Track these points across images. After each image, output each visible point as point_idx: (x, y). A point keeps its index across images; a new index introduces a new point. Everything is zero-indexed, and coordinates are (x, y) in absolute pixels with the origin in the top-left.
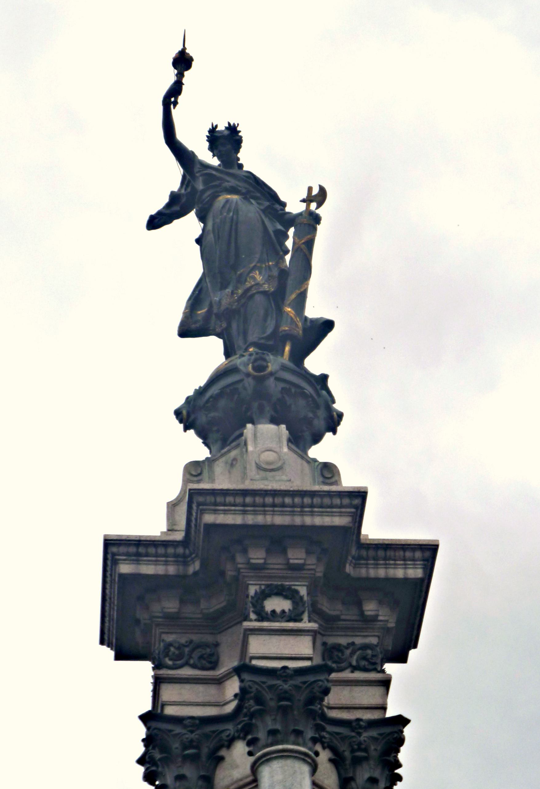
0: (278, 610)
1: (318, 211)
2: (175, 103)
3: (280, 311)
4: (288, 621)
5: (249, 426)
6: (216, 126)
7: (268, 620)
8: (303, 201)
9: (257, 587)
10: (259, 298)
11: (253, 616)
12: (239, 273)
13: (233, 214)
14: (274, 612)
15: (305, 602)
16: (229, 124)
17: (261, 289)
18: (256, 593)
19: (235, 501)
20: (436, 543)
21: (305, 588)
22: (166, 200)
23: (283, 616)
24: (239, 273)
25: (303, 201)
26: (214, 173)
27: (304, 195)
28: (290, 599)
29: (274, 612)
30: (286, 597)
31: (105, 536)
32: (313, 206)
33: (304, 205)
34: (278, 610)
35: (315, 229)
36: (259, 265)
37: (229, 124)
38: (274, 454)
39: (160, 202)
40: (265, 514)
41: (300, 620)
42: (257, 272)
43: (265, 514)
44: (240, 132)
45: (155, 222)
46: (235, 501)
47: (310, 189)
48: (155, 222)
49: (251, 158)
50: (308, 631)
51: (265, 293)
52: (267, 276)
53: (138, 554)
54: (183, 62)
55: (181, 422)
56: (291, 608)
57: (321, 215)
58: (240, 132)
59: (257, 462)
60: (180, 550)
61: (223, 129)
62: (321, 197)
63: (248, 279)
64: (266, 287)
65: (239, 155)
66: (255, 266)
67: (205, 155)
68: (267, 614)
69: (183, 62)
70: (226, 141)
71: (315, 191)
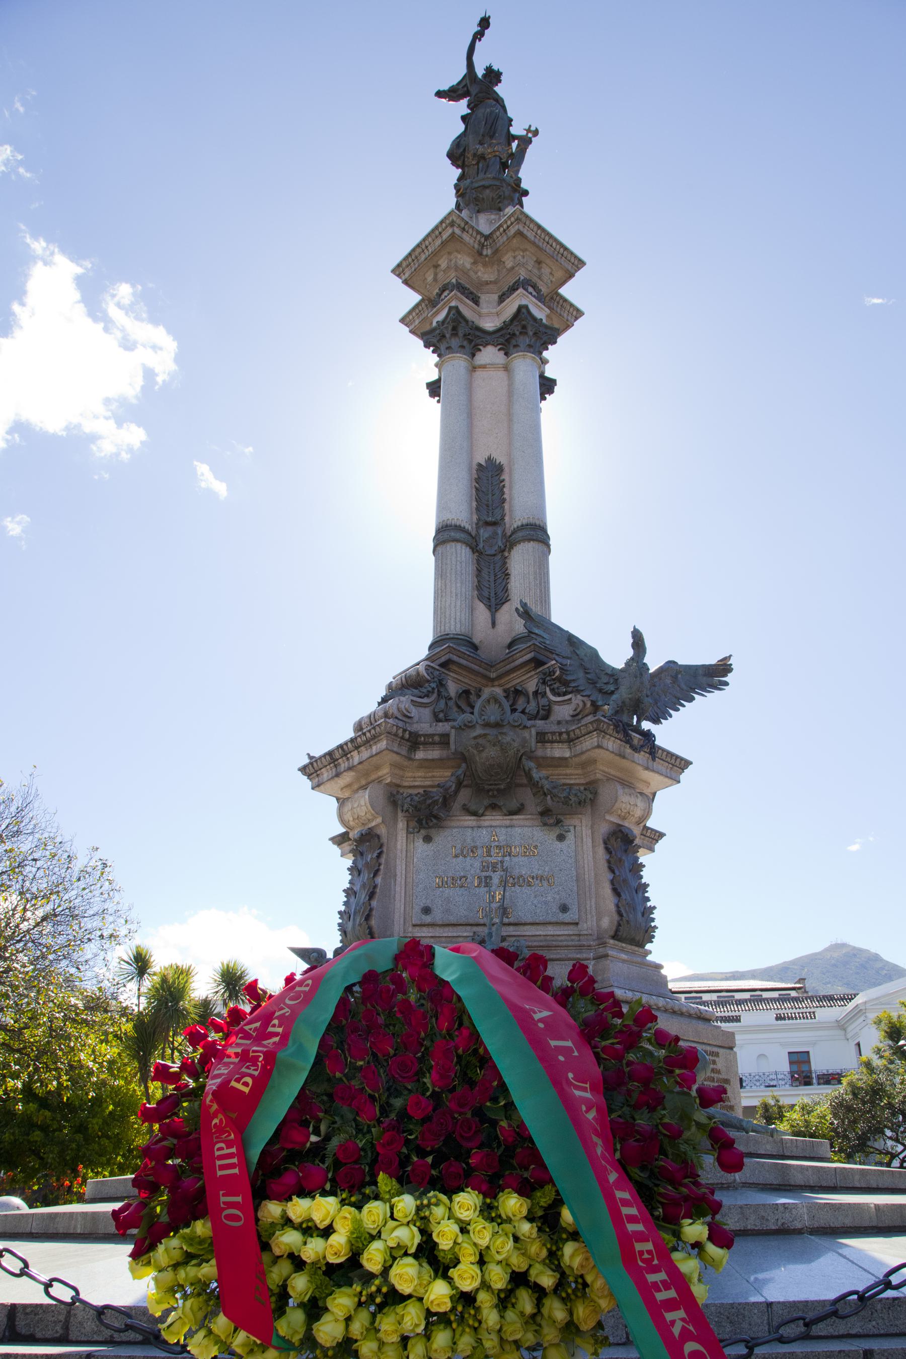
39: (445, 87)
48: (440, 94)
70: (493, 76)
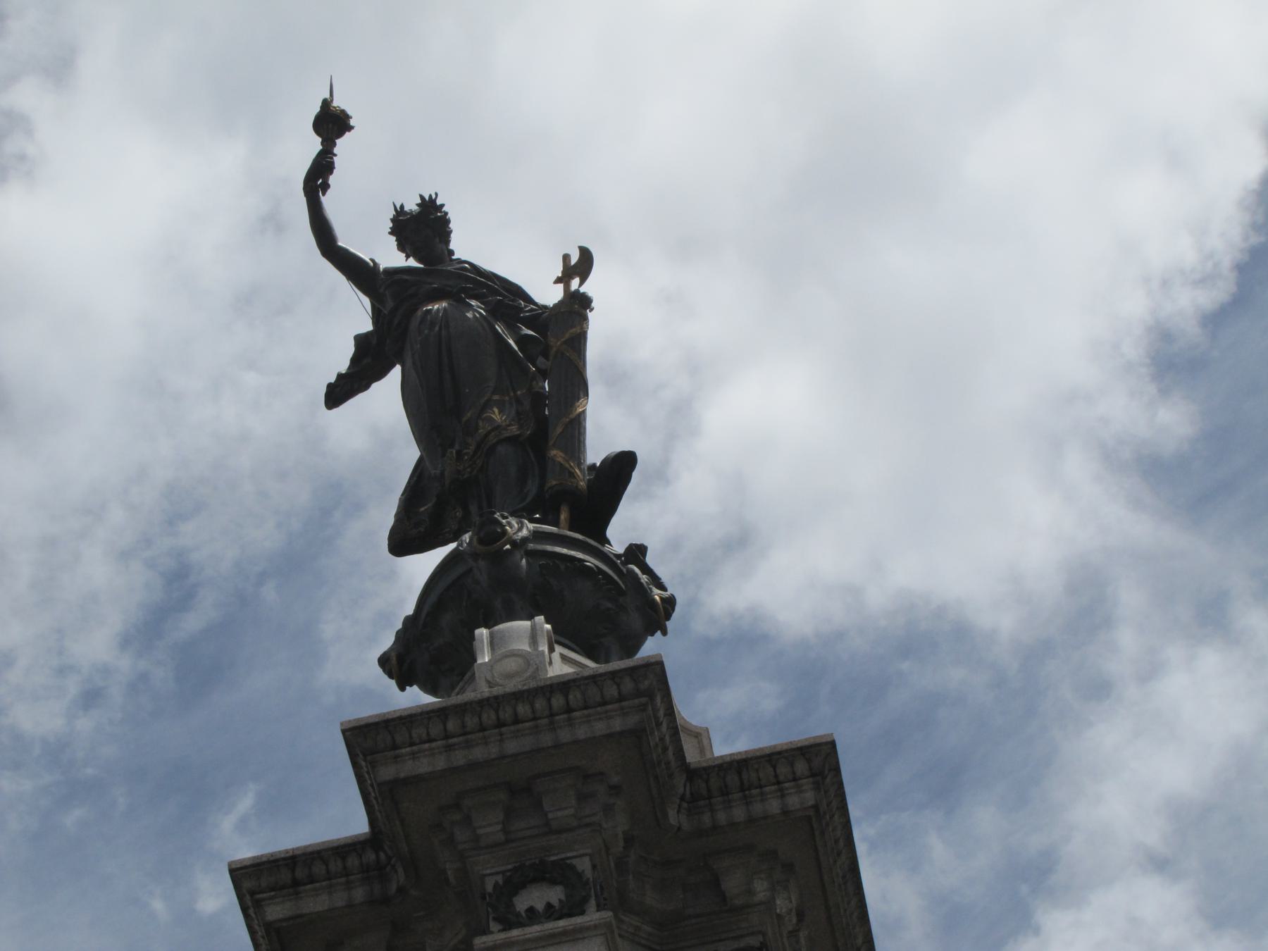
0: (540, 906)
1: (582, 290)
2: (325, 187)
3: (542, 458)
4: (560, 918)
5: (482, 633)
6: (402, 207)
7: (521, 925)
8: (558, 281)
9: (500, 879)
10: (502, 449)
11: (494, 926)
12: (464, 419)
13: (440, 328)
14: (531, 910)
15: (587, 883)
16: (422, 197)
17: (506, 434)
18: (496, 885)
19: (428, 734)
20: (829, 739)
21: (587, 859)
22: (350, 350)
23: (551, 912)
24: (464, 419)
25: (558, 281)
26: (405, 277)
27: (558, 272)
28: (560, 883)
29: (531, 910)
30: (553, 882)
31: (230, 864)
32: (575, 284)
33: (561, 286)
34: (540, 906)
35: (585, 319)
36: (496, 397)
37: (422, 197)
38: (520, 661)
39: (340, 359)
40: (486, 744)
41: (582, 913)
42: (496, 410)
43: (486, 744)
44: (442, 206)
45: (338, 394)
46: (428, 734)
47: (566, 258)
48: (338, 394)
49: (469, 244)
50: (596, 927)
51: (512, 440)
52: (513, 412)
53: (296, 883)
54: (331, 123)
55: (391, 676)
56: (563, 898)
57: (590, 294)
58: (442, 206)
59: (489, 678)
60: (370, 856)
61: (415, 208)
62: (581, 266)
63: (481, 424)
64: (514, 429)
65: (338, 141)
66: (489, 400)
67: (388, 255)
68: (518, 915)
69: (331, 123)
70: (423, 227)
71: (574, 259)
